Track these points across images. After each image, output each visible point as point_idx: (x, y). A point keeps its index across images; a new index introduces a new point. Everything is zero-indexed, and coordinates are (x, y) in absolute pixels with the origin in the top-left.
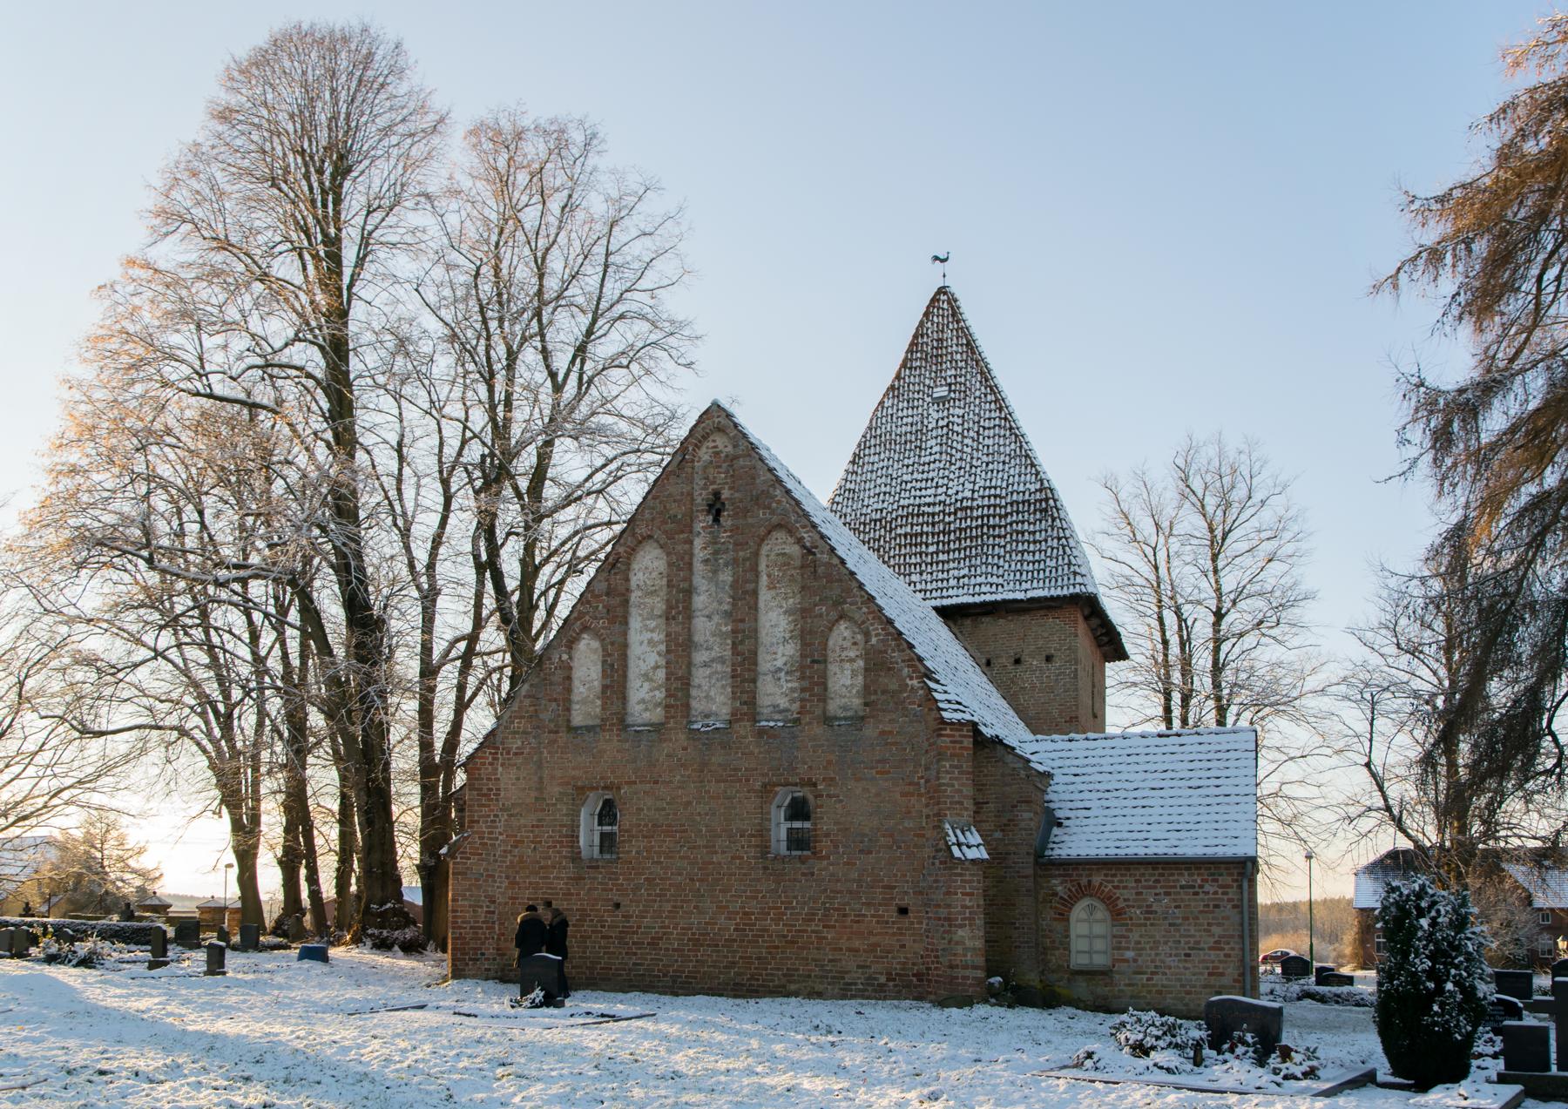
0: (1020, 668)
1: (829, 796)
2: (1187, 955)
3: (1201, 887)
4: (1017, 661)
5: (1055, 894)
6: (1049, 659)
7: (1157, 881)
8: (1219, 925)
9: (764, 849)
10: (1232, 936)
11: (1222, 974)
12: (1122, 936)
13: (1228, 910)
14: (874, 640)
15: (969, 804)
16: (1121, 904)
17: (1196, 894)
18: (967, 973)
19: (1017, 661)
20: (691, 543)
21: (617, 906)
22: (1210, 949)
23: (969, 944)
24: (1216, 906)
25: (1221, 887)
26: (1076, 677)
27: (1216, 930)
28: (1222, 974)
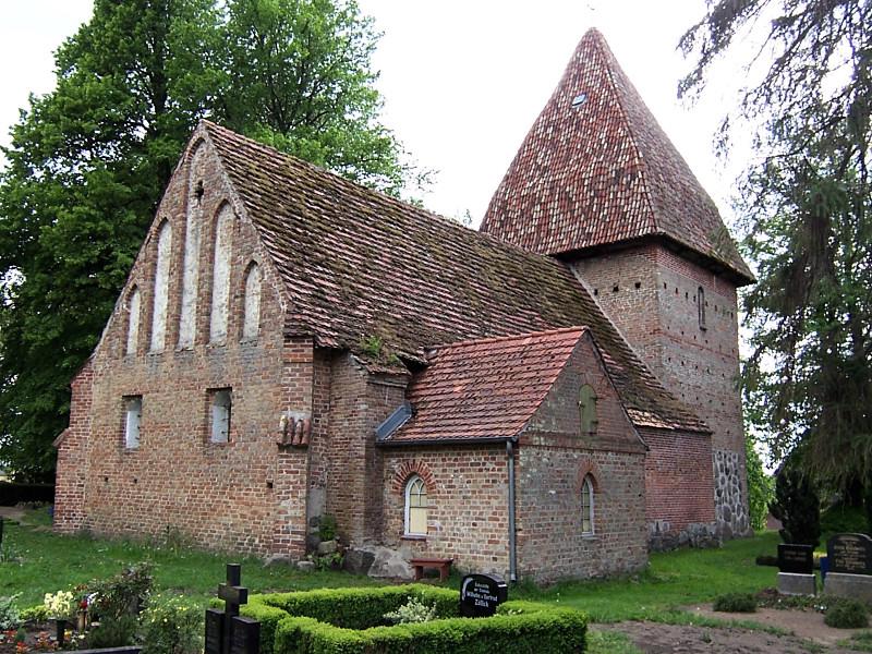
0: (619, 294)
1: (238, 397)
2: (474, 524)
3: (484, 464)
4: (616, 289)
5: (393, 472)
6: (638, 286)
7: (456, 460)
8: (496, 498)
9: (206, 439)
10: (503, 508)
11: (497, 542)
12: (433, 507)
13: (503, 487)
14: (266, 277)
15: (308, 400)
16: (433, 480)
17: (481, 470)
18: (287, 537)
19: (616, 289)
20: (186, 219)
21: (136, 481)
22: (490, 519)
23: (291, 513)
24: (494, 481)
25: (497, 464)
26: (657, 298)
27: (494, 503)
28: (497, 542)
